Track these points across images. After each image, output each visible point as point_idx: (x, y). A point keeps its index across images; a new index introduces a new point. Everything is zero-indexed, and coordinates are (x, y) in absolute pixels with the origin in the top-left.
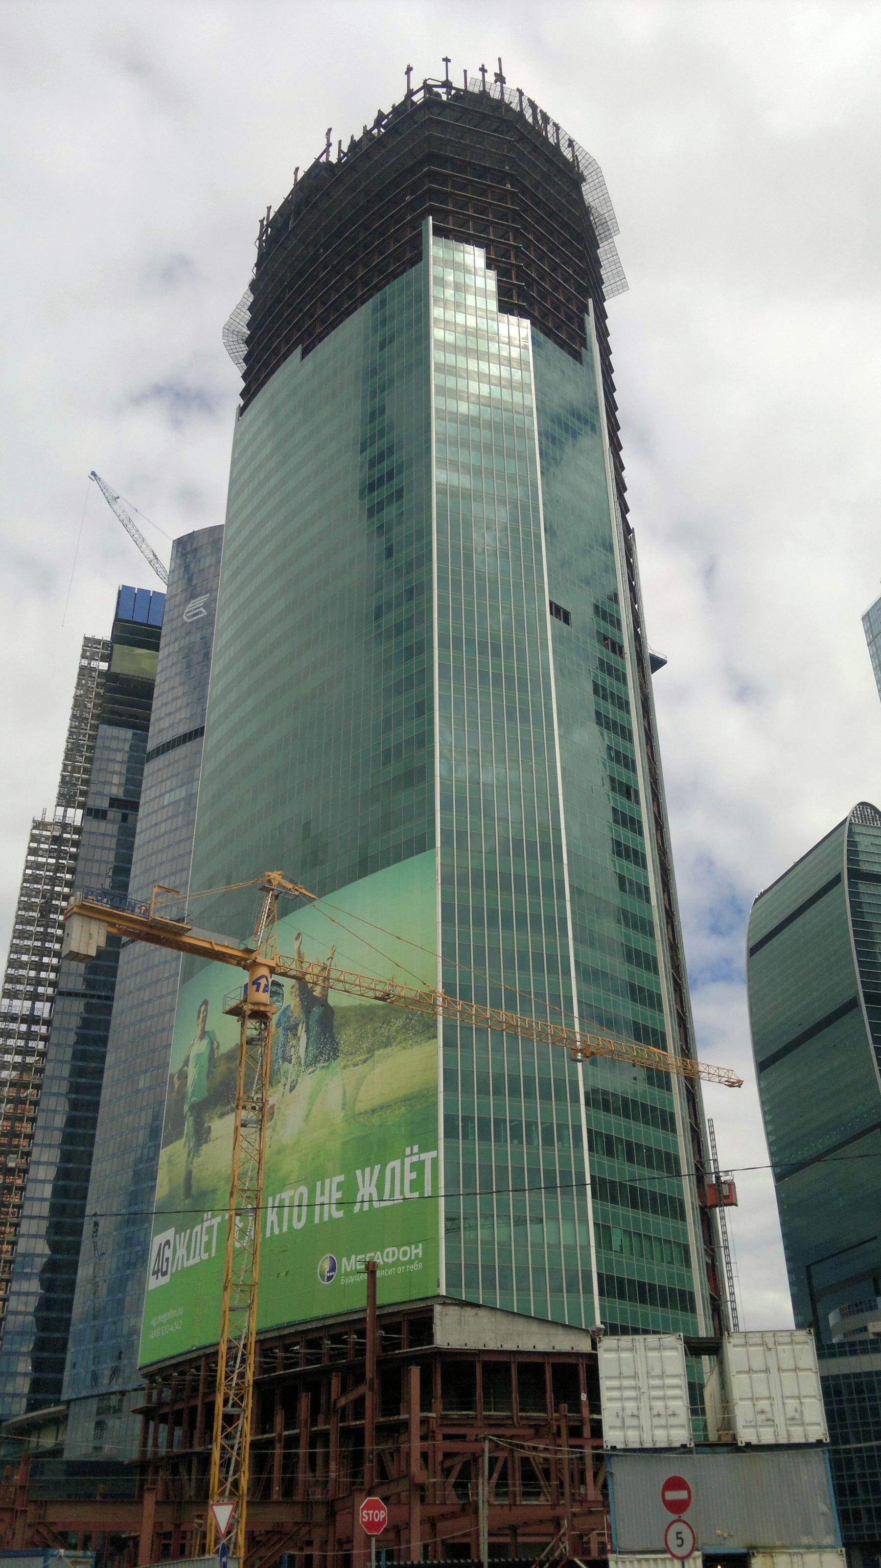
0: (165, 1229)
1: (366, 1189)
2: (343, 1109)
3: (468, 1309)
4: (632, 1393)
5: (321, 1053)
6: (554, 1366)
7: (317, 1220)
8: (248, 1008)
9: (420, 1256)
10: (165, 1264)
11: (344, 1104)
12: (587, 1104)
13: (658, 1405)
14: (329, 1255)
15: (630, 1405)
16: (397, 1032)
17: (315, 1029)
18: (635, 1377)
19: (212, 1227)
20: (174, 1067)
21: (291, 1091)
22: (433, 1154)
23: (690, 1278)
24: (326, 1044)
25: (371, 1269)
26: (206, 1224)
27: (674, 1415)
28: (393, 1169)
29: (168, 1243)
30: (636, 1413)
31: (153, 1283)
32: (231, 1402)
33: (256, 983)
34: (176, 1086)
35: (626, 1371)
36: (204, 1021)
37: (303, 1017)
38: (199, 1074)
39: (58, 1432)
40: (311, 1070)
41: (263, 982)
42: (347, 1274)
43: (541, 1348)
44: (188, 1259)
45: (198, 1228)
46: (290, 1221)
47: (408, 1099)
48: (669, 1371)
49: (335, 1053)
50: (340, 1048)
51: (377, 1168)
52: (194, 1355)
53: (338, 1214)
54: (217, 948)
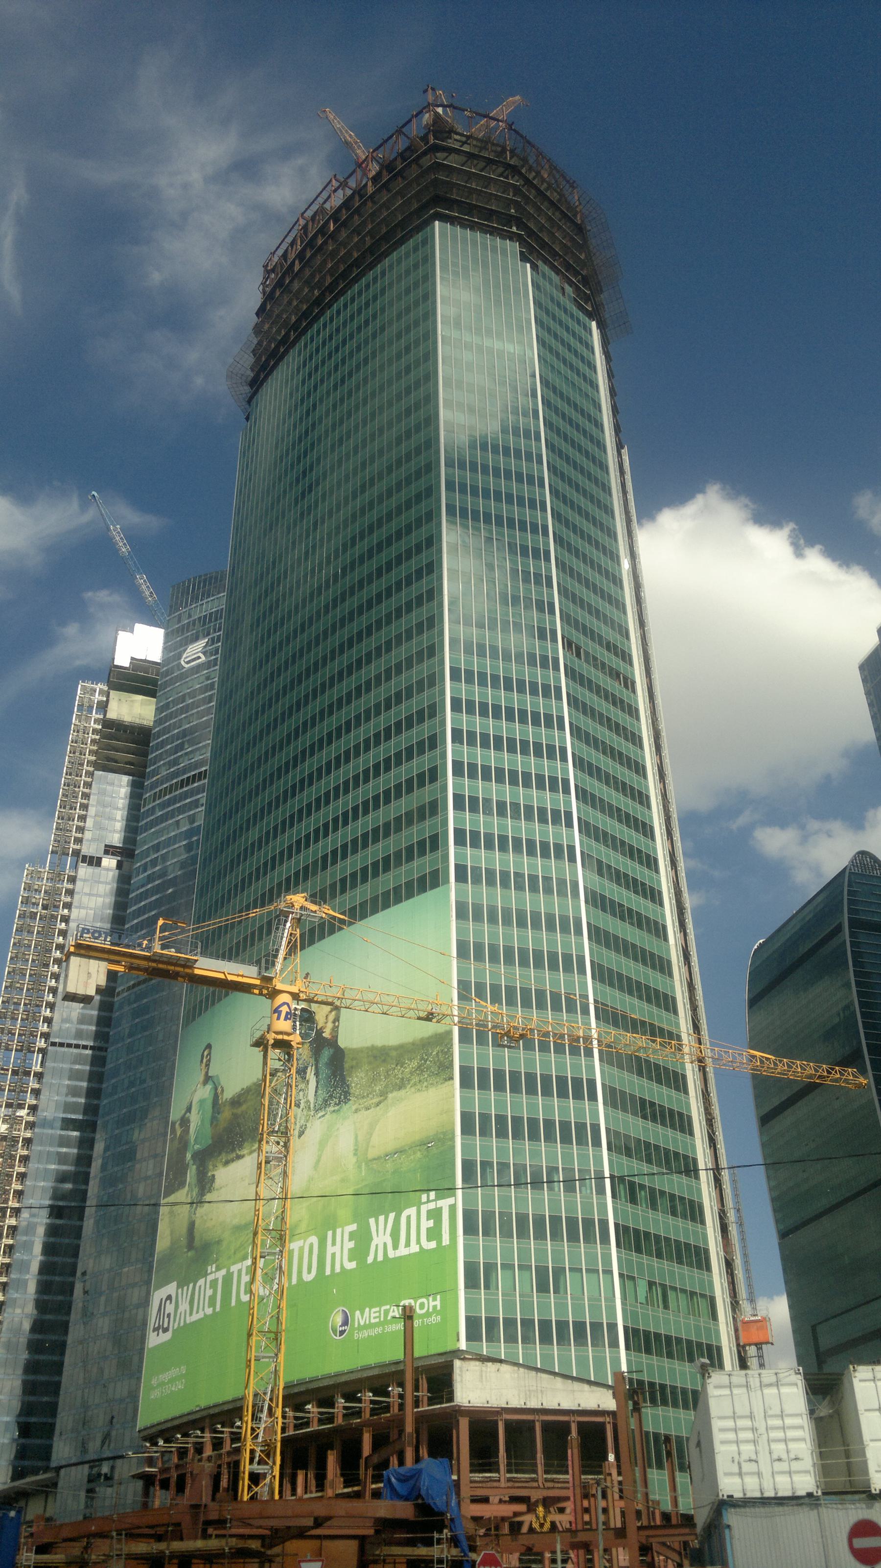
0: (167, 1283)
1: (380, 1238)
2: (355, 1154)
3: (490, 1364)
4: (749, 1435)
5: (331, 1096)
6: (580, 1425)
7: (328, 1272)
8: (271, 1038)
9: (439, 1308)
10: (166, 1320)
11: (356, 1150)
12: (609, 1149)
13: (779, 1449)
14: (341, 1308)
15: (747, 1449)
16: (411, 1073)
17: (325, 1072)
18: (751, 1417)
19: (216, 1280)
20: (175, 1114)
21: (300, 1136)
22: (451, 1201)
23: (717, 1332)
24: (336, 1087)
25: (408, 1315)
26: (210, 1278)
27: (797, 1459)
28: (409, 1217)
29: (169, 1298)
30: (754, 1457)
31: (154, 1340)
32: (257, 1459)
33: (277, 1011)
34: (178, 1133)
35: (739, 1411)
36: (208, 1065)
37: (312, 1061)
38: (202, 1121)
39: (46, 1502)
40: (321, 1114)
41: (285, 1009)
42: (361, 1328)
43: (566, 1405)
44: (191, 1314)
45: (201, 1282)
46: (300, 1272)
47: (423, 1144)
48: (788, 1410)
49: (345, 1096)
50: (352, 1091)
51: (392, 1216)
52: (198, 1416)
53: (351, 1265)
54: (230, 978)
